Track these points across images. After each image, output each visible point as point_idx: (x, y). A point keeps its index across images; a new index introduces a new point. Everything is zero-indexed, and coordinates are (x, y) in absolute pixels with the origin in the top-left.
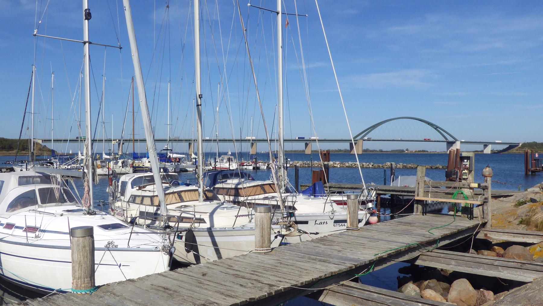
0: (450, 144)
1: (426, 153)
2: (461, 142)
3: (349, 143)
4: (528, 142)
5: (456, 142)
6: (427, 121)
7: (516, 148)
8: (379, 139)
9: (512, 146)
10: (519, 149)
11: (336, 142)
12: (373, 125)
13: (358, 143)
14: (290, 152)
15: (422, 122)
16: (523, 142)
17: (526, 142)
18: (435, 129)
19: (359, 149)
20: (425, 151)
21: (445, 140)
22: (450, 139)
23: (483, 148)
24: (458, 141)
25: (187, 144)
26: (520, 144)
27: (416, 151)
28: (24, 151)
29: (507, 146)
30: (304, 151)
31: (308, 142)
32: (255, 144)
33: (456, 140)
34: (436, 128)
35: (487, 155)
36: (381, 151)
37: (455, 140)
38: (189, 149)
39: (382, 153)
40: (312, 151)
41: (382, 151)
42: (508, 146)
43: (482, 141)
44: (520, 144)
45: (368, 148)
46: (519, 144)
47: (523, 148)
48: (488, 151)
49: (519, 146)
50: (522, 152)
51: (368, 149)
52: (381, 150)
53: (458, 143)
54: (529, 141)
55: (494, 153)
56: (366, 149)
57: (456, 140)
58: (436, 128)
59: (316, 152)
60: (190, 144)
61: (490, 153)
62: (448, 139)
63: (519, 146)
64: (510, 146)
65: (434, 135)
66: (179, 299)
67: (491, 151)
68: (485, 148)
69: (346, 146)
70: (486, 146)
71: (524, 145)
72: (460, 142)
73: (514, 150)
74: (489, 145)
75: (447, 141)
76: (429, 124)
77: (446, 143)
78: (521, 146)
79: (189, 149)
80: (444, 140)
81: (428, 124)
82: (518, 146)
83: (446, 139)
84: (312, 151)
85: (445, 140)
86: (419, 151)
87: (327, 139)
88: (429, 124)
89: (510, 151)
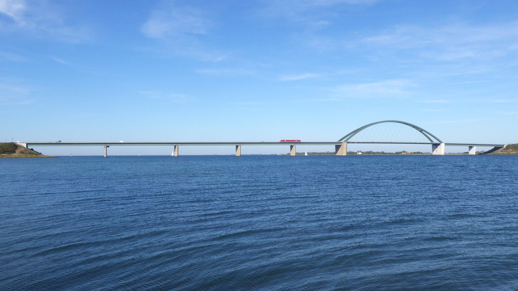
0: (435, 146)
1: (421, 154)
2: (445, 144)
3: (335, 146)
4: (513, 144)
5: (440, 144)
6: (416, 126)
7: (501, 149)
8: (415, 142)
9: (497, 148)
10: (503, 150)
11: (270, 144)
12: (358, 128)
13: (342, 145)
14: (302, 154)
15: (407, 125)
16: (507, 144)
17: (511, 144)
18: (420, 131)
19: (344, 151)
20: (419, 153)
21: (430, 142)
22: (436, 141)
23: (468, 149)
24: (443, 143)
25: (235, 146)
26: (505, 146)
27: (411, 153)
28: (4, 153)
29: (493, 147)
30: (290, 154)
31: (292, 144)
32: (239, 147)
33: (441, 142)
34: (421, 131)
35: (472, 156)
36: (383, 153)
37: (439, 142)
38: (291, 151)
39: (383, 154)
40: (296, 153)
41: (384, 153)
42: (494, 147)
43: (467, 143)
44: (505, 146)
45: (371, 150)
46: (504, 145)
47: (507, 150)
48: (473, 152)
49: (504, 148)
50: (506, 153)
51: (372, 151)
52: (383, 152)
53: (443, 145)
54: (514, 143)
55: (480, 154)
56: (369, 151)
57: (441, 142)
58: (421, 131)
59: (325, 154)
60: (237, 147)
61: (475, 154)
62: (433, 142)
63: (504, 148)
64: (495, 147)
65: (421, 138)
66: (329, 289)
67: (476, 152)
68: (470, 150)
69: (332, 149)
70: (471, 148)
71: (509, 147)
72: (444, 144)
73: (499, 152)
74: (473, 146)
75: (433, 143)
76: (414, 127)
77: (431, 145)
78: (506, 147)
79: (291, 151)
80: (430, 142)
81: (413, 127)
82: (502, 147)
83: (432, 141)
84: (347, 153)
85: (430, 142)
86: (415, 153)
87: (265, 141)
88: (414, 127)
89: (495, 152)
